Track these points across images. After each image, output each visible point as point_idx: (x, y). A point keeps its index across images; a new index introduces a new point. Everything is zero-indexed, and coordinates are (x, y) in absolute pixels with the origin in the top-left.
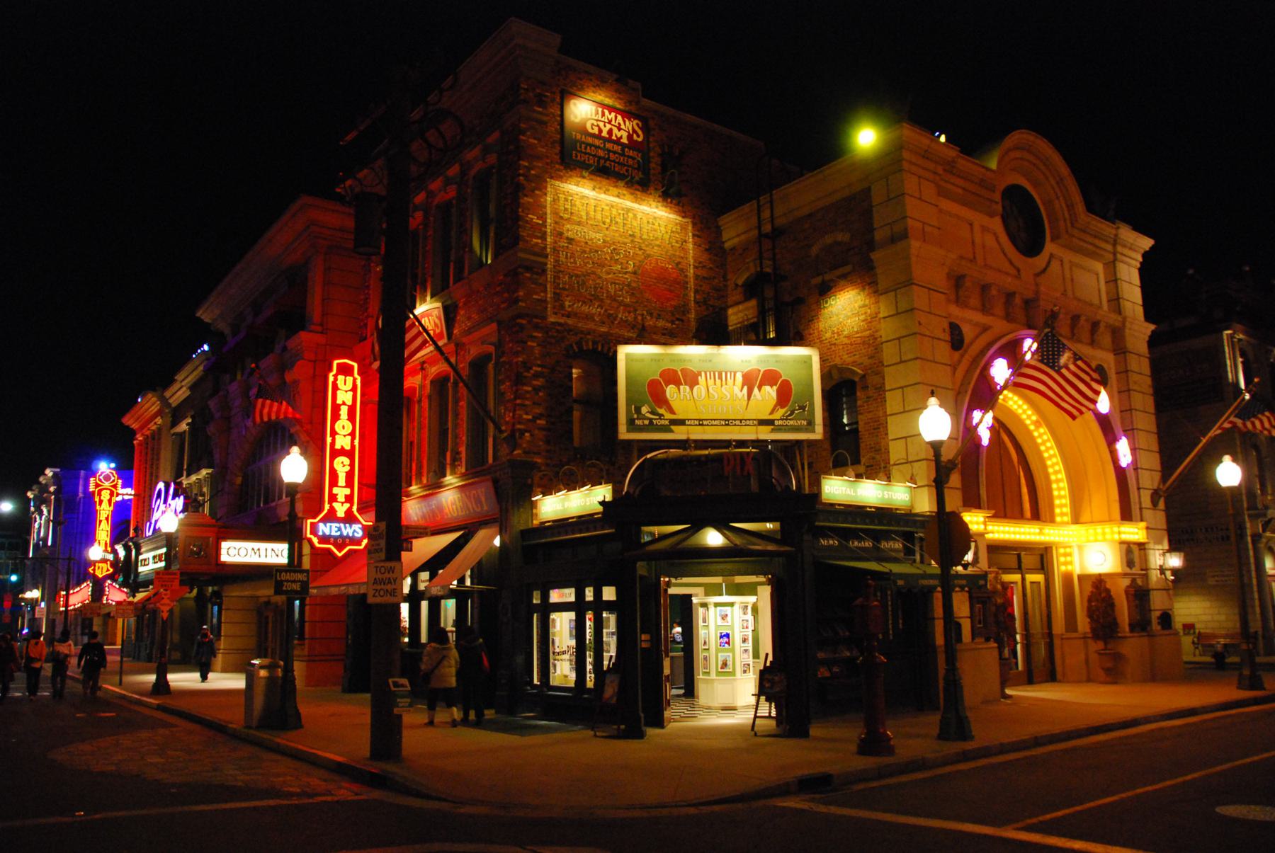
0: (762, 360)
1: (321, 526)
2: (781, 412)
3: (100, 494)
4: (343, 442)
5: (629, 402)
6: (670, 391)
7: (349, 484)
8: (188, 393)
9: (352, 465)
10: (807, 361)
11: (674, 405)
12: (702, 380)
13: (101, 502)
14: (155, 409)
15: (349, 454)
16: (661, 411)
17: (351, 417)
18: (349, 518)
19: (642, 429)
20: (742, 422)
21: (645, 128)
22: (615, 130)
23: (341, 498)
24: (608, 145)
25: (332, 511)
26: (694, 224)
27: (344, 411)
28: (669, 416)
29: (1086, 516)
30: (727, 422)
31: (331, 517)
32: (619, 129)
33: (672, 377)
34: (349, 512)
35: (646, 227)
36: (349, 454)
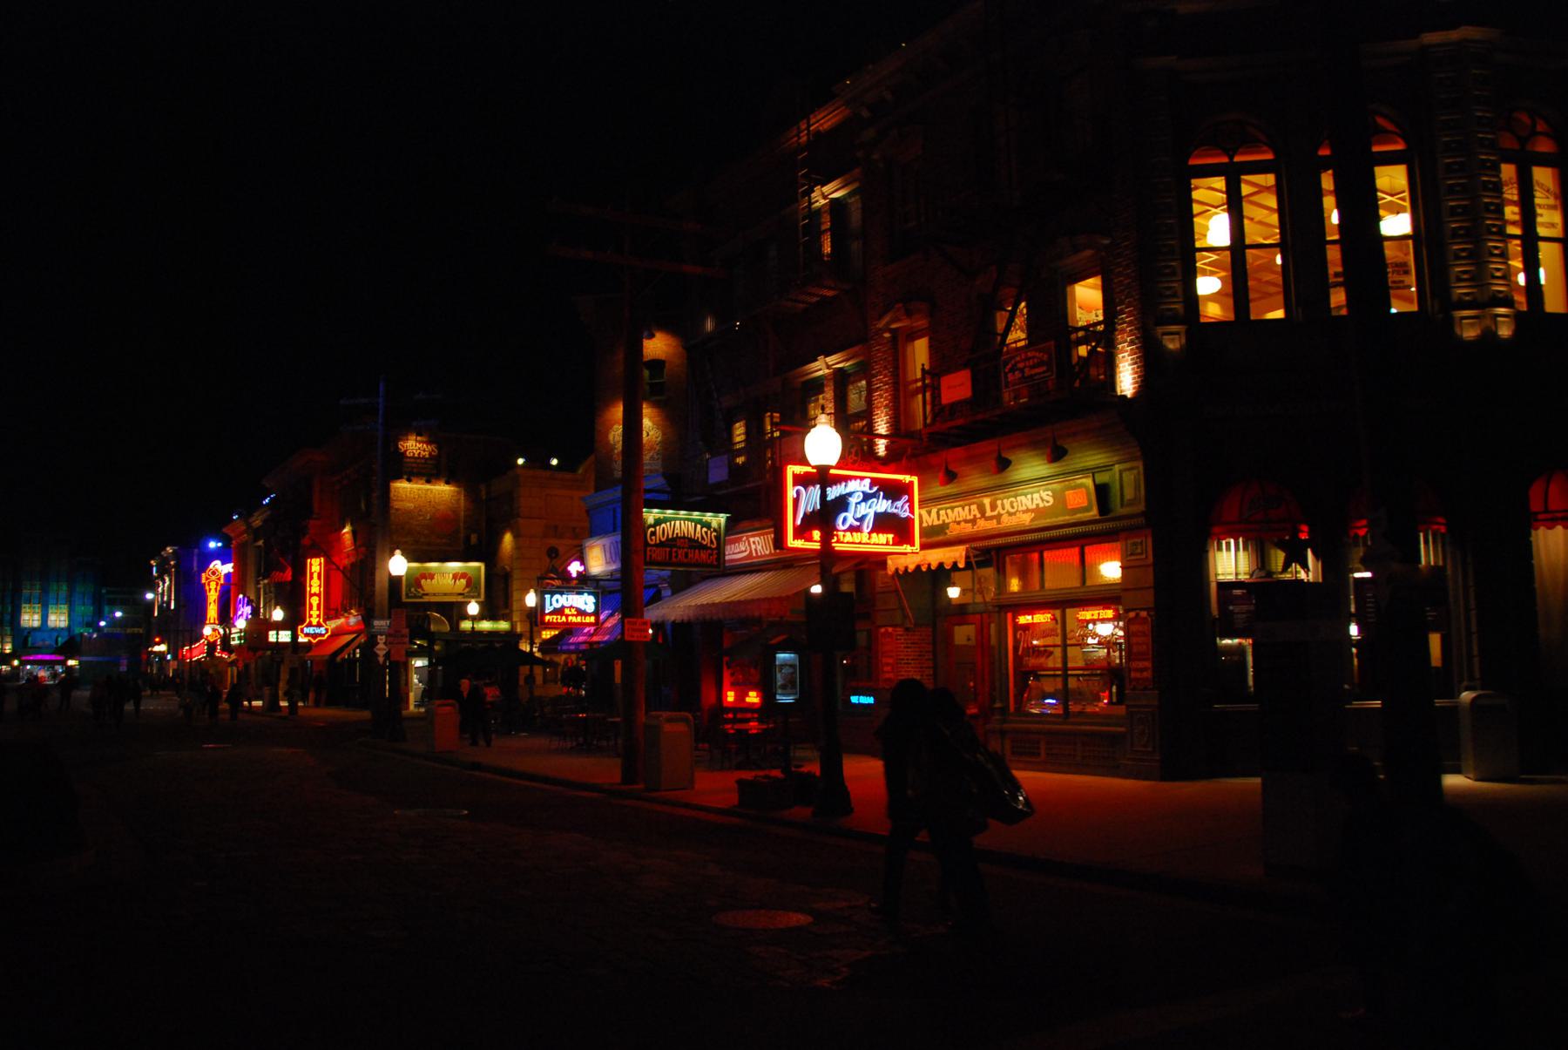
0: (460, 568)
1: (305, 629)
2: (467, 590)
3: (209, 585)
4: (315, 589)
5: (407, 586)
6: (423, 581)
7: (319, 608)
8: (260, 524)
9: (320, 600)
10: (479, 568)
11: (425, 588)
12: (436, 577)
13: (210, 590)
14: (244, 528)
15: (318, 595)
16: (419, 590)
17: (319, 578)
18: (319, 625)
19: (412, 597)
20: (451, 594)
21: (439, 448)
22: (422, 452)
23: (315, 616)
24: (418, 461)
25: (310, 622)
26: (465, 490)
27: (315, 575)
28: (422, 592)
29: (1125, 571)
30: (445, 594)
31: (310, 625)
32: (424, 451)
33: (424, 576)
34: (319, 622)
35: (437, 496)
36: (318, 595)
